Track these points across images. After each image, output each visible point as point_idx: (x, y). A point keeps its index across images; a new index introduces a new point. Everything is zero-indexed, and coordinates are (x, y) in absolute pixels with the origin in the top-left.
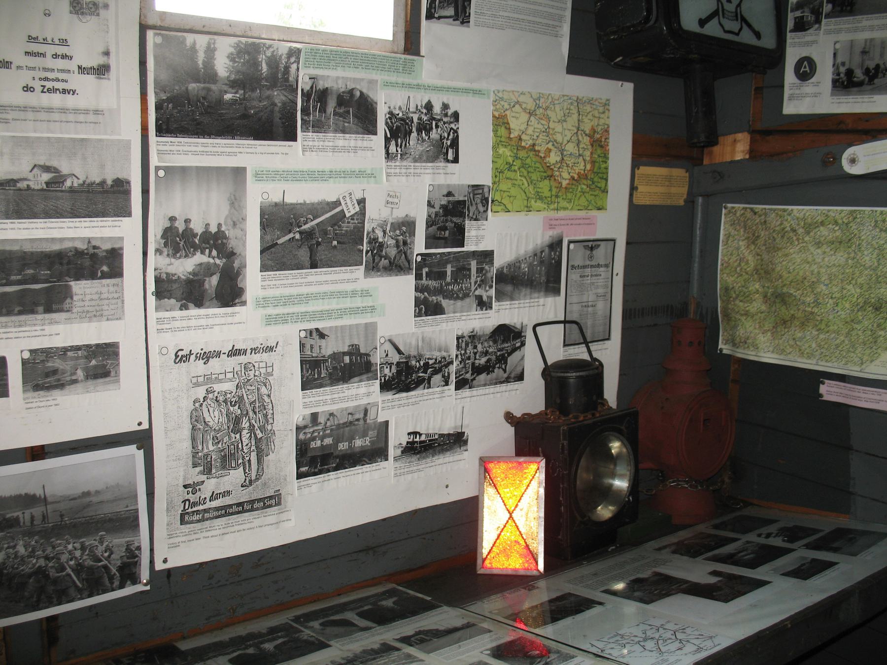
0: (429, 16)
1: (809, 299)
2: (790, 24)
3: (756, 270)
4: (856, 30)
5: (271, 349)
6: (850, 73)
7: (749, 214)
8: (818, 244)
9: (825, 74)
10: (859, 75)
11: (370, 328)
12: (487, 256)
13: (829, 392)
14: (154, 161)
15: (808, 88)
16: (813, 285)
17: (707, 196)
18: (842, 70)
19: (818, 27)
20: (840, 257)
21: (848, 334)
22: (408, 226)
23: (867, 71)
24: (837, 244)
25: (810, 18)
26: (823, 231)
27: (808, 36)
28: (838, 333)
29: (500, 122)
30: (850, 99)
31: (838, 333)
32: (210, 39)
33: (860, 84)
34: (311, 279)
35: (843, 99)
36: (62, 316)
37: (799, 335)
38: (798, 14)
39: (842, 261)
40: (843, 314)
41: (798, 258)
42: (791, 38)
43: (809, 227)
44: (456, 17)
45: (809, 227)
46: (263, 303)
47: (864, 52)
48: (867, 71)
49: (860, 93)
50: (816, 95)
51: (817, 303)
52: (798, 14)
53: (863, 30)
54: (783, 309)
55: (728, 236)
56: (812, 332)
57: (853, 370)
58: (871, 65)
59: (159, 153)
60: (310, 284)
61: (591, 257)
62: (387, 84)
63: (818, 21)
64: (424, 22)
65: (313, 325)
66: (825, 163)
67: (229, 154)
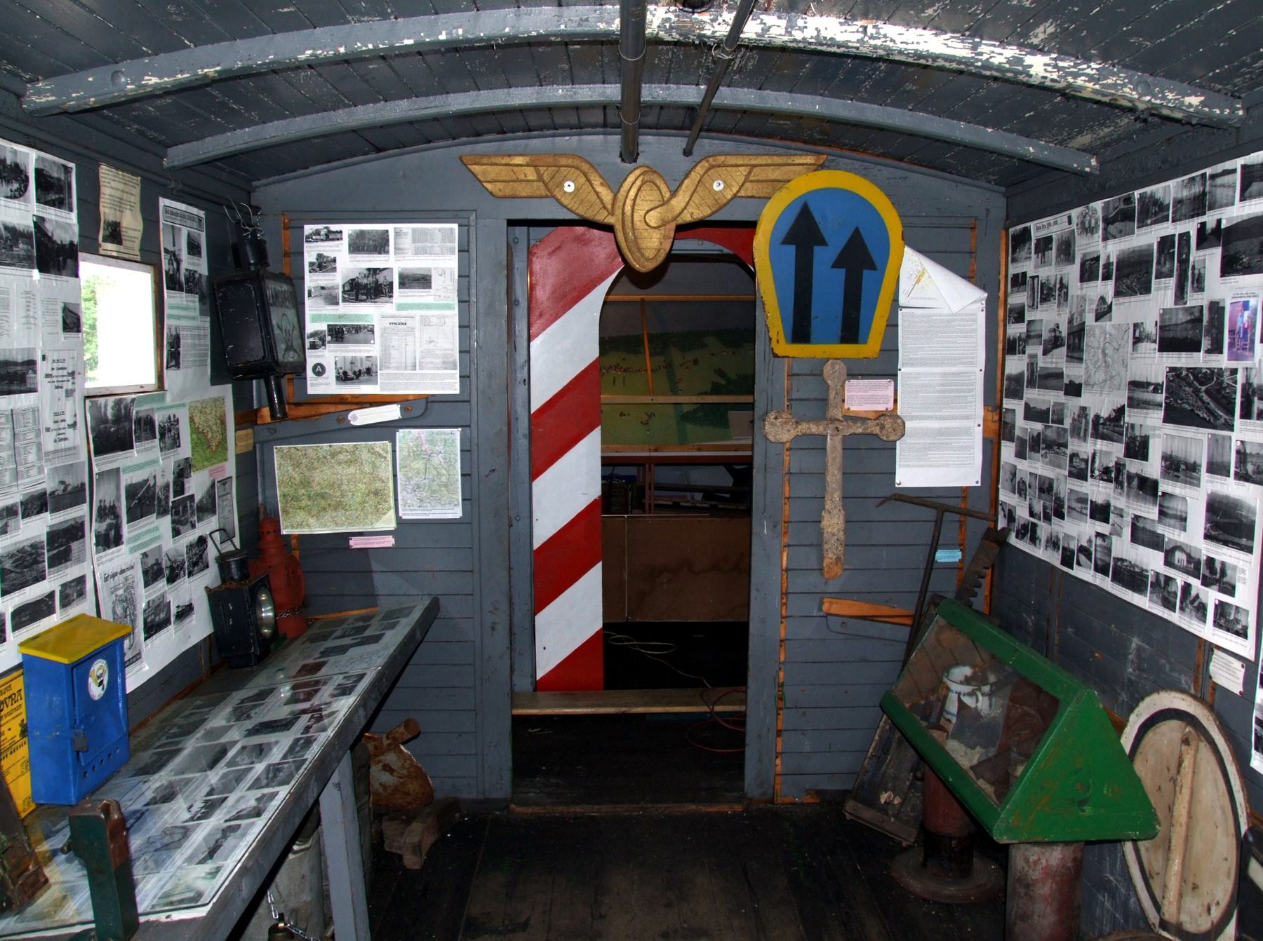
0: (167, 368)
1: (338, 494)
2: (307, 345)
3: (301, 482)
4: (346, 351)
5: (132, 567)
6: (345, 373)
7: (293, 451)
8: (340, 464)
9: (331, 373)
10: (351, 374)
11: (160, 547)
12: (192, 497)
13: (355, 543)
14: (96, 470)
15: (321, 380)
16: (339, 486)
17: (260, 443)
18: (341, 371)
19: (19, 190)
20: (352, 470)
21: (362, 510)
22: (167, 486)
23: (355, 373)
24: (350, 463)
25: (319, 343)
26: (341, 457)
27: (319, 352)
28: (356, 510)
29: (192, 419)
30: (347, 386)
31: (356, 510)
32: (1247, 612)
33: (352, 379)
34: (142, 524)
35: (342, 386)
36: (69, 563)
37: (334, 514)
38: (312, 340)
39: (353, 471)
40: (358, 500)
41: (329, 472)
42: (309, 353)
43: (334, 455)
44: (175, 366)
45: (334, 455)
46: (131, 540)
47: (352, 363)
48: (355, 373)
49: (353, 383)
50: (327, 384)
51: (343, 496)
52: (312, 340)
53: (350, 351)
54: (323, 502)
55: (280, 465)
56: (340, 512)
57: (368, 528)
58: (357, 370)
59: (97, 465)
60: (140, 528)
61: (225, 490)
62: (158, 409)
63: (324, 344)
64: (165, 370)
65: (143, 551)
66: (339, 421)
67: (112, 462)
